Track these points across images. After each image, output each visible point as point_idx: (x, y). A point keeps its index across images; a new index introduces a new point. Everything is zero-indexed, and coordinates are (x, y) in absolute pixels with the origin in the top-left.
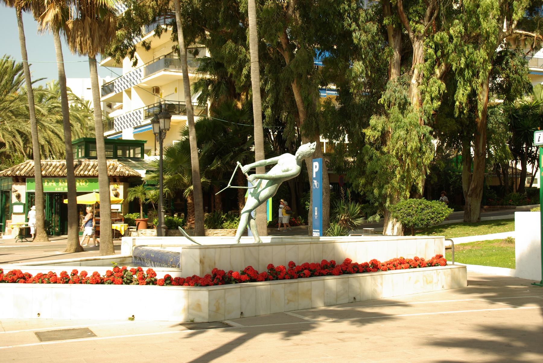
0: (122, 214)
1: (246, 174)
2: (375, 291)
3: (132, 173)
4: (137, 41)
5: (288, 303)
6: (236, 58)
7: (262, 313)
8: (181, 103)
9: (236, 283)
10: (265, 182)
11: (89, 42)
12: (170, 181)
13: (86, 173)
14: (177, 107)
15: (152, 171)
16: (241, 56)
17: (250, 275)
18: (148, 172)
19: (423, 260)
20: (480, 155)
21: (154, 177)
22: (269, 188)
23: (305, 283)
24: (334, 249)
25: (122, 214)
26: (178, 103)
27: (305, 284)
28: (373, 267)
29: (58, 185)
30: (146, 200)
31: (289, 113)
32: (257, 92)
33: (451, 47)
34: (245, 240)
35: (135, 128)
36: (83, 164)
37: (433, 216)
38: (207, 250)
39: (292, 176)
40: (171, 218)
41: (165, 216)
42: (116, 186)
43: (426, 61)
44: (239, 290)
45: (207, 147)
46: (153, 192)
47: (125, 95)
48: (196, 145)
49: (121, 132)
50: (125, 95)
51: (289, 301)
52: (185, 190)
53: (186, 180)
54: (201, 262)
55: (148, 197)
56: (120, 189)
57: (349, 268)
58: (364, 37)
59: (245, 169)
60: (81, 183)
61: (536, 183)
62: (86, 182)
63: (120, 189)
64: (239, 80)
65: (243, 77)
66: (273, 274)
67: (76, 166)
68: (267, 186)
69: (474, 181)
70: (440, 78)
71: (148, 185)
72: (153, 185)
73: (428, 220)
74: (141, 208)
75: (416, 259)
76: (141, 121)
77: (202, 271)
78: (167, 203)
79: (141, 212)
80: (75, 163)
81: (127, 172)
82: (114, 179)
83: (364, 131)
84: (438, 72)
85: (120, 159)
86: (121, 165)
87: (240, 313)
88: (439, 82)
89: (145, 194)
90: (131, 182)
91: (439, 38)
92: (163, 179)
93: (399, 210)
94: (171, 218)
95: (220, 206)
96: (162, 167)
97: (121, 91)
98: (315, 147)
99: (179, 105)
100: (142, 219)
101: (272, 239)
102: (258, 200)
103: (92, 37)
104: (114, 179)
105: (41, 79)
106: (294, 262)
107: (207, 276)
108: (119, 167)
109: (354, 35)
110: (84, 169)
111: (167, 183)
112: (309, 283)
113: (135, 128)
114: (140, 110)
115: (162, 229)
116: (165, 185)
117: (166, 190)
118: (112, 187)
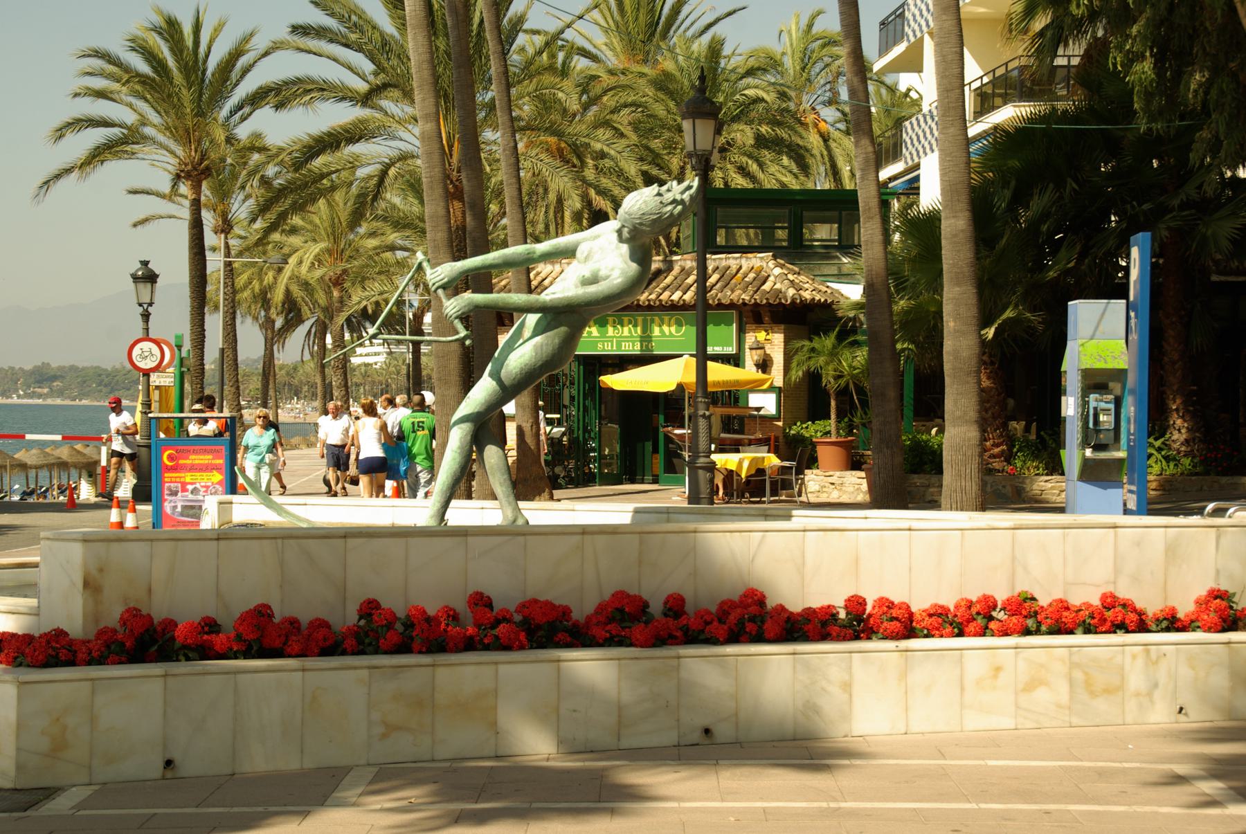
0: (780, 424)
2: (811, 709)
3: (807, 295)
5: (384, 736)
7: (258, 761)
9: (188, 659)
13: (676, 297)
17: (265, 635)
19: (1063, 606)
22: (538, 339)
25: (780, 424)
27: (464, 673)
28: (855, 623)
29: (603, 335)
31: (1216, 71)
34: (464, 514)
36: (677, 269)
38: (115, 546)
42: (762, 336)
44: (160, 681)
49: (917, 167)
51: (391, 729)
54: (86, 584)
56: (775, 344)
57: (755, 619)
60: (665, 328)
62: (679, 324)
63: (775, 344)
66: (381, 632)
67: (659, 273)
74: (833, 403)
75: (1110, 601)
77: (93, 615)
79: (833, 416)
80: (654, 266)
81: (791, 292)
82: (755, 314)
85: (779, 253)
86: (777, 271)
87: (161, 765)
97: (919, 35)
98: (686, 196)
101: (637, 511)
102: (500, 382)
104: (755, 314)
105: (729, 14)
106: (488, 591)
108: (779, 278)
110: (675, 284)
112: (488, 671)
115: (701, 472)
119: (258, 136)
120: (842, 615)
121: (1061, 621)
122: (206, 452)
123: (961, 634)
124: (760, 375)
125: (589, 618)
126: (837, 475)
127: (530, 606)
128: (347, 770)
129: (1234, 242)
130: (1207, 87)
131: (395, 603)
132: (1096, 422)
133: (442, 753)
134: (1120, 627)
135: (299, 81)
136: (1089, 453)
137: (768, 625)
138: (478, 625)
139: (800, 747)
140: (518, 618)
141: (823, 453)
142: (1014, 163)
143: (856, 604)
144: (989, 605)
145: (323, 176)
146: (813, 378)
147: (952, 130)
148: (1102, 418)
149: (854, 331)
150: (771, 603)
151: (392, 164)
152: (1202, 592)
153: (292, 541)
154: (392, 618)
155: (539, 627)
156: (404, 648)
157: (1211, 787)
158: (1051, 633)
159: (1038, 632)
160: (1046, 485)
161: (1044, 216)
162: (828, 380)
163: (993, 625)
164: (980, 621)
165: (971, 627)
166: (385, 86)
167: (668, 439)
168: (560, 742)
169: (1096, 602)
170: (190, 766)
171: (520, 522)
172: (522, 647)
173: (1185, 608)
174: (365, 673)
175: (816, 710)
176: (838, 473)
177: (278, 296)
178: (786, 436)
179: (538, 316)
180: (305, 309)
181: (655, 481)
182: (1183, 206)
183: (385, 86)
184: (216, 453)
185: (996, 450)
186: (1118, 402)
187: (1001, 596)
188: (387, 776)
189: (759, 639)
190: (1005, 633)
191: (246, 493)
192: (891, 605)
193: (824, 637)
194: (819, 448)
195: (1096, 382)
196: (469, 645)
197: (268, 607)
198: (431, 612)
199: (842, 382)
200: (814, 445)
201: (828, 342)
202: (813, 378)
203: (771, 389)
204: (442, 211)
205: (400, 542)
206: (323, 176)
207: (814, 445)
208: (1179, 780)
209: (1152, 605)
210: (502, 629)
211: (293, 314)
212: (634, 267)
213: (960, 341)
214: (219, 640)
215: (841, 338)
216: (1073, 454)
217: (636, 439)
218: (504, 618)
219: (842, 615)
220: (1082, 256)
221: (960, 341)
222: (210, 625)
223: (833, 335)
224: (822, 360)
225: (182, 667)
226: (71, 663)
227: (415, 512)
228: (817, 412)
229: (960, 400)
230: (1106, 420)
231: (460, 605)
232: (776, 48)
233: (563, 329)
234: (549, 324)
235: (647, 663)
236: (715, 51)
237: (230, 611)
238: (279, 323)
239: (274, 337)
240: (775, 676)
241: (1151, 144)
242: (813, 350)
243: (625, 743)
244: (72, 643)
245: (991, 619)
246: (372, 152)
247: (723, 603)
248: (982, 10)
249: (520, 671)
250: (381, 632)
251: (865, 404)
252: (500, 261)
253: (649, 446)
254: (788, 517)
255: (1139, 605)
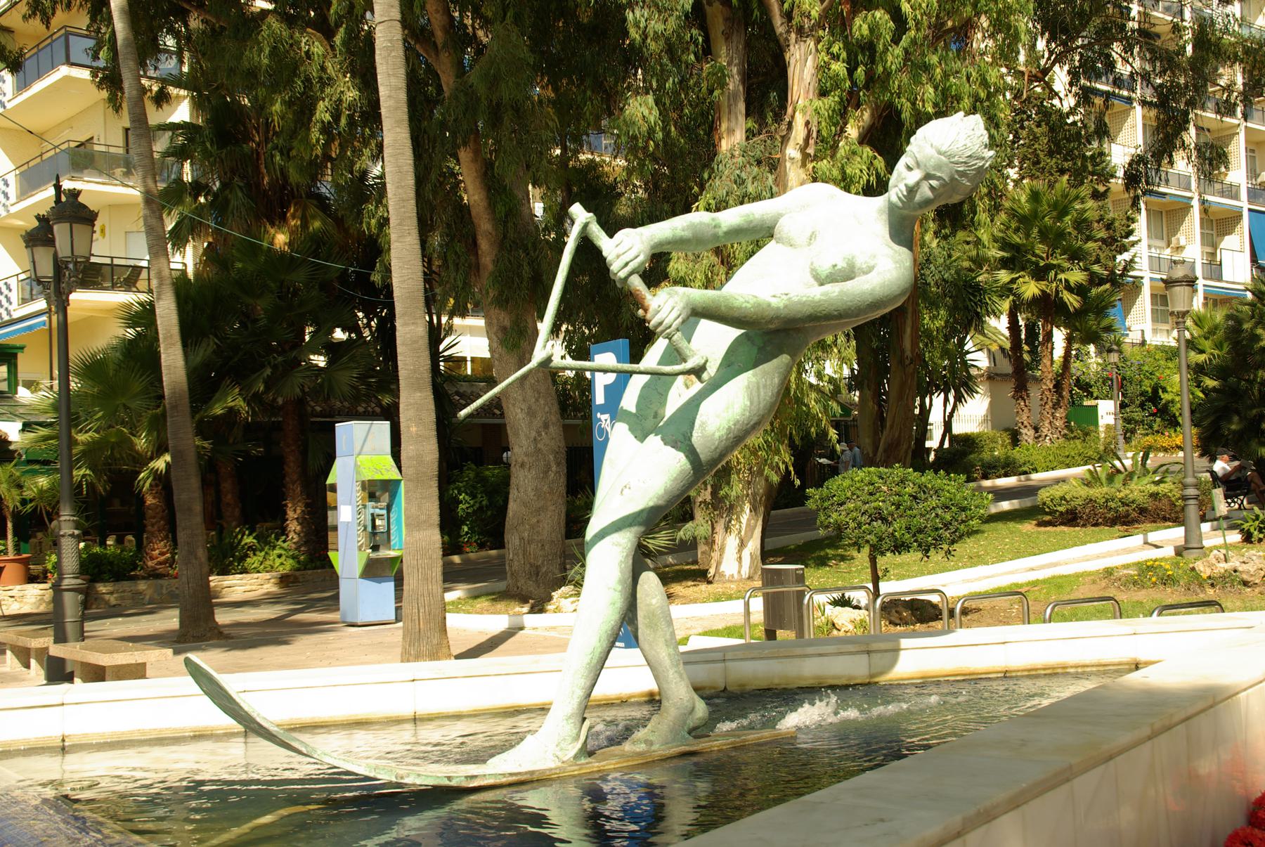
1: (637, 283)
6: (294, 68)
8: (116, 262)
12: (91, 453)
14: (107, 270)
15: (41, 424)
18: (27, 427)
20: (907, 362)
21: (46, 439)
26: (108, 261)
30: (24, 502)
32: (398, 122)
33: (894, 56)
37: (948, 517)
39: (875, 305)
40: (97, 549)
41: (82, 545)
43: (823, 93)
45: (205, 351)
46: (43, 482)
48: (176, 330)
52: (139, 473)
53: (142, 443)
55: (28, 494)
58: (656, 26)
59: (625, 250)
61: (931, 439)
64: (306, 139)
65: (315, 134)
68: (733, 365)
69: (892, 427)
70: (862, 140)
71: (29, 462)
72: (46, 463)
73: (937, 529)
74: (10, 525)
76: (10, 308)
78: (86, 510)
79: (10, 536)
84: (852, 131)
88: (867, 151)
89: (20, 487)
91: (865, 27)
92: (72, 442)
93: (842, 504)
94: (97, 549)
95: (237, 512)
96: (68, 410)
99: (112, 265)
100: (11, 556)
102: (692, 453)
109: (630, 16)
111: (83, 454)
114: (9, 281)
116: (78, 460)
117: (82, 472)
126: (17, 589)
147: (409, 239)
148: (378, 522)
176: (19, 587)
185: (163, 558)
191: (576, 757)
212: (904, 253)
234: (761, 349)
248: (20, 223)
252: (687, 234)
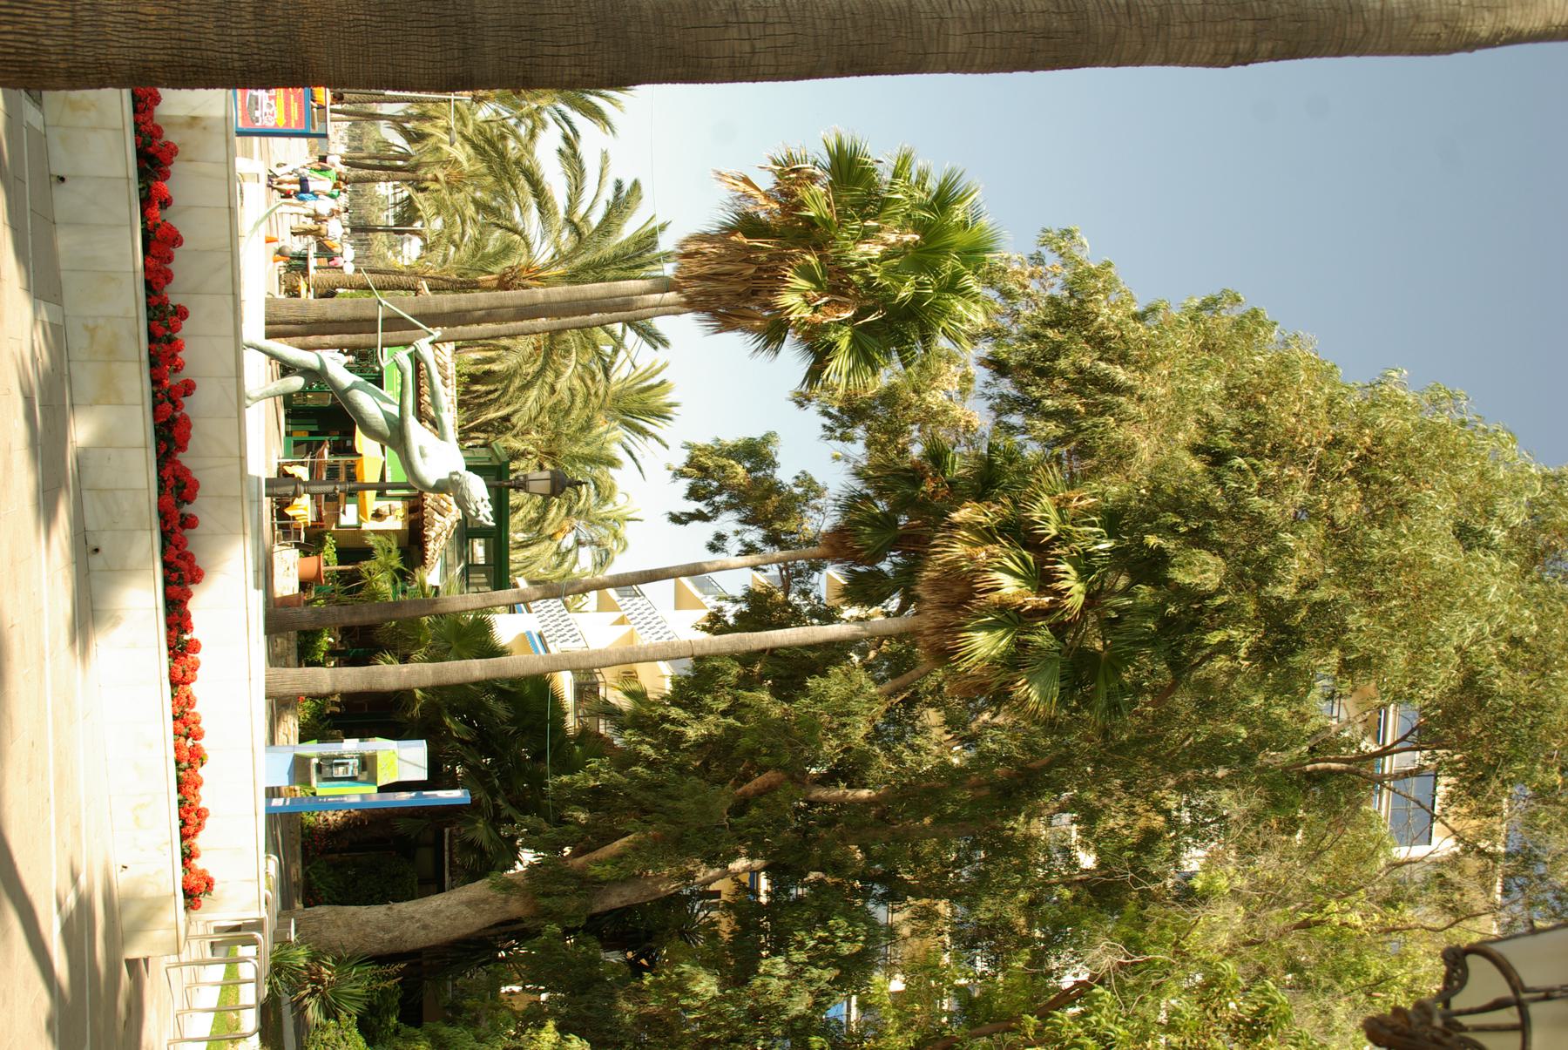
3: (430, 546)
4: (728, 522)
5: (86, 327)
7: (65, 241)
10: (395, 411)
11: (705, 270)
16: (708, 699)
17: (160, 244)
22: (381, 418)
23: (138, 386)
24: (230, 532)
27: (136, 383)
28: (180, 647)
35: (540, 636)
42: (400, 513)
44: (122, 173)
47: (616, 616)
50: (616, 616)
51: (92, 332)
54: (194, 118)
57: (181, 576)
63: (395, 522)
66: (164, 325)
68: (386, 415)
77: (171, 122)
81: (432, 534)
82: (416, 509)
83: (551, 1024)
87: (61, 174)
90: (413, 544)
98: (481, 518)
102: (350, 388)
103: (714, 277)
104: (416, 509)
106: (196, 393)
107: (157, 131)
109: (779, 959)
112: (138, 399)
113: (540, 636)
118: (399, 506)
119: (544, 126)
120: (186, 637)
121: (186, 785)
122: (300, 114)
123: (175, 718)
124: (370, 513)
125: (178, 463)
127: (186, 423)
128: (60, 303)
129: (472, 841)
130: (576, 822)
131: (187, 329)
132: (338, 765)
133: (75, 367)
134: (184, 823)
135: (582, 171)
136: (315, 761)
137: (178, 589)
138: (172, 388)
139: (87, 615)
140: (178, 414)
141: (312, 563)
142: (527, 689)
143: (194, 646)
144: (197, 736)
145: (513, 186)
146: (367, 553)
148: (341, 769)
149: (404, 580)
150: (193, 588)
151: (520, 234)
152: (211, 874)
153: (229, 258)
154: (176, 329)
155: (171, 430)
156: (152, 338)
157: (71, 902)
158: (178, 777)
159: (179, 770)
160: (290, 726)
161: (491, 713)
162: (365, 565)
163: (182, 740)
164: (185, 731)
165: (179, 725)
166: (579, 234)
167: (321, 444)
168: (85, 449)
169: (201, 805)
170: (62, 195)
171: (248, 402)
172: (155, 418)
173: (198, 864)
174: (134, 314)
175: (115, 625)
177: (427, 127)
178: (325, 533)
179: (397, 414)
180: (419, 146)
181: (287, 434)
182: (496, 807)
183: (579, 234)
184: (298, 123)
186: (353, 779)
187: (202, 743)
188: (57, 336)
189: (166, 582)
190: (177, 748)
192: (194, 670)
193: (170, 626)
194: (315, 558)
195: (367, 764)
196: (156, 382)
197: (181, 244)
198: (180, 354)
199: (366, 575)
200: (318, 553)
201: (396, 563)
202: (367, 553)
203: (360, 521)
204: (481, 305)
205: (230, 330)
206: (513, 186)
207: (318, 553)
208: (75, 879)
209: (200, 842)
210: (168, 406)
211: (415, 137)
212: (432, 482)
213: (388, 674)
214: (156, 212)
215: (399, 571)
216: (313, 749)
217: (321, 420)
218: (177, 405)
219: (186, 637)
220: (461, 741)
221: (388, 674)
222: (166, 203)
223: (400, 566)
224: (382, 558)
225: (134, 187)
226: (136, 111)
227: (253, 327)
228: (344, 555)
229: (351, 678)
230: (340, 772)
231: (185, 374)
232: (619, 498)
233: (388, 433)
235: (146, 513)
236: (612, 462)
237: (174, 218)
238: (408, 126)
239: (397, 122)
240: (140, 599)
241: (538, 782)
242: (390, 551)
243: (85, 494)
244: (151, 110)
245: (187, 738)
246: (531, 222)
247: (192, 555)
249: (138, 426)
250: (164, 325)
251: (349, 592)
253: (315, 428)
254: (257, 587)
255: (201, 834)
